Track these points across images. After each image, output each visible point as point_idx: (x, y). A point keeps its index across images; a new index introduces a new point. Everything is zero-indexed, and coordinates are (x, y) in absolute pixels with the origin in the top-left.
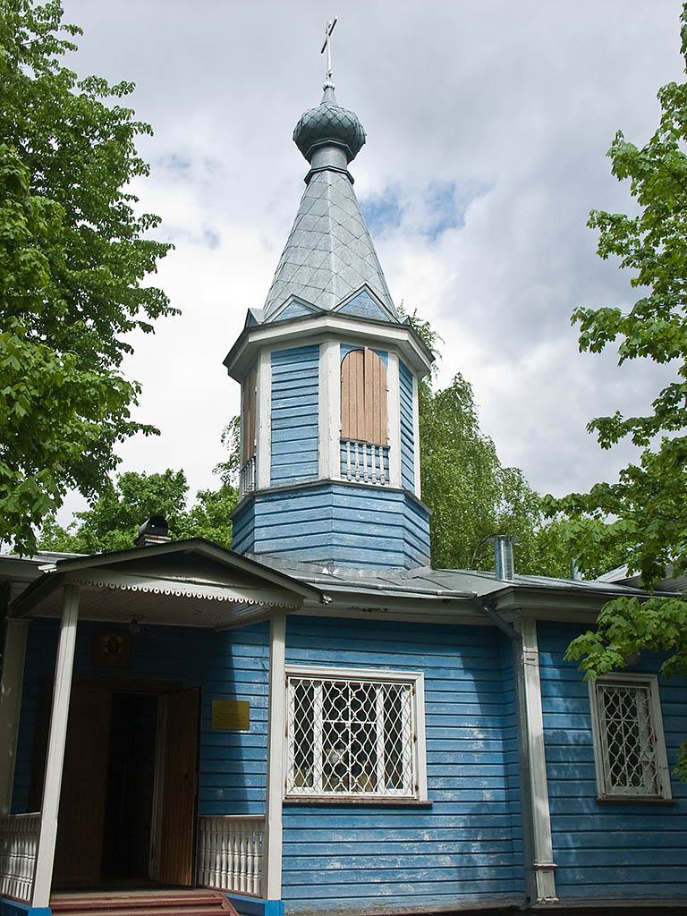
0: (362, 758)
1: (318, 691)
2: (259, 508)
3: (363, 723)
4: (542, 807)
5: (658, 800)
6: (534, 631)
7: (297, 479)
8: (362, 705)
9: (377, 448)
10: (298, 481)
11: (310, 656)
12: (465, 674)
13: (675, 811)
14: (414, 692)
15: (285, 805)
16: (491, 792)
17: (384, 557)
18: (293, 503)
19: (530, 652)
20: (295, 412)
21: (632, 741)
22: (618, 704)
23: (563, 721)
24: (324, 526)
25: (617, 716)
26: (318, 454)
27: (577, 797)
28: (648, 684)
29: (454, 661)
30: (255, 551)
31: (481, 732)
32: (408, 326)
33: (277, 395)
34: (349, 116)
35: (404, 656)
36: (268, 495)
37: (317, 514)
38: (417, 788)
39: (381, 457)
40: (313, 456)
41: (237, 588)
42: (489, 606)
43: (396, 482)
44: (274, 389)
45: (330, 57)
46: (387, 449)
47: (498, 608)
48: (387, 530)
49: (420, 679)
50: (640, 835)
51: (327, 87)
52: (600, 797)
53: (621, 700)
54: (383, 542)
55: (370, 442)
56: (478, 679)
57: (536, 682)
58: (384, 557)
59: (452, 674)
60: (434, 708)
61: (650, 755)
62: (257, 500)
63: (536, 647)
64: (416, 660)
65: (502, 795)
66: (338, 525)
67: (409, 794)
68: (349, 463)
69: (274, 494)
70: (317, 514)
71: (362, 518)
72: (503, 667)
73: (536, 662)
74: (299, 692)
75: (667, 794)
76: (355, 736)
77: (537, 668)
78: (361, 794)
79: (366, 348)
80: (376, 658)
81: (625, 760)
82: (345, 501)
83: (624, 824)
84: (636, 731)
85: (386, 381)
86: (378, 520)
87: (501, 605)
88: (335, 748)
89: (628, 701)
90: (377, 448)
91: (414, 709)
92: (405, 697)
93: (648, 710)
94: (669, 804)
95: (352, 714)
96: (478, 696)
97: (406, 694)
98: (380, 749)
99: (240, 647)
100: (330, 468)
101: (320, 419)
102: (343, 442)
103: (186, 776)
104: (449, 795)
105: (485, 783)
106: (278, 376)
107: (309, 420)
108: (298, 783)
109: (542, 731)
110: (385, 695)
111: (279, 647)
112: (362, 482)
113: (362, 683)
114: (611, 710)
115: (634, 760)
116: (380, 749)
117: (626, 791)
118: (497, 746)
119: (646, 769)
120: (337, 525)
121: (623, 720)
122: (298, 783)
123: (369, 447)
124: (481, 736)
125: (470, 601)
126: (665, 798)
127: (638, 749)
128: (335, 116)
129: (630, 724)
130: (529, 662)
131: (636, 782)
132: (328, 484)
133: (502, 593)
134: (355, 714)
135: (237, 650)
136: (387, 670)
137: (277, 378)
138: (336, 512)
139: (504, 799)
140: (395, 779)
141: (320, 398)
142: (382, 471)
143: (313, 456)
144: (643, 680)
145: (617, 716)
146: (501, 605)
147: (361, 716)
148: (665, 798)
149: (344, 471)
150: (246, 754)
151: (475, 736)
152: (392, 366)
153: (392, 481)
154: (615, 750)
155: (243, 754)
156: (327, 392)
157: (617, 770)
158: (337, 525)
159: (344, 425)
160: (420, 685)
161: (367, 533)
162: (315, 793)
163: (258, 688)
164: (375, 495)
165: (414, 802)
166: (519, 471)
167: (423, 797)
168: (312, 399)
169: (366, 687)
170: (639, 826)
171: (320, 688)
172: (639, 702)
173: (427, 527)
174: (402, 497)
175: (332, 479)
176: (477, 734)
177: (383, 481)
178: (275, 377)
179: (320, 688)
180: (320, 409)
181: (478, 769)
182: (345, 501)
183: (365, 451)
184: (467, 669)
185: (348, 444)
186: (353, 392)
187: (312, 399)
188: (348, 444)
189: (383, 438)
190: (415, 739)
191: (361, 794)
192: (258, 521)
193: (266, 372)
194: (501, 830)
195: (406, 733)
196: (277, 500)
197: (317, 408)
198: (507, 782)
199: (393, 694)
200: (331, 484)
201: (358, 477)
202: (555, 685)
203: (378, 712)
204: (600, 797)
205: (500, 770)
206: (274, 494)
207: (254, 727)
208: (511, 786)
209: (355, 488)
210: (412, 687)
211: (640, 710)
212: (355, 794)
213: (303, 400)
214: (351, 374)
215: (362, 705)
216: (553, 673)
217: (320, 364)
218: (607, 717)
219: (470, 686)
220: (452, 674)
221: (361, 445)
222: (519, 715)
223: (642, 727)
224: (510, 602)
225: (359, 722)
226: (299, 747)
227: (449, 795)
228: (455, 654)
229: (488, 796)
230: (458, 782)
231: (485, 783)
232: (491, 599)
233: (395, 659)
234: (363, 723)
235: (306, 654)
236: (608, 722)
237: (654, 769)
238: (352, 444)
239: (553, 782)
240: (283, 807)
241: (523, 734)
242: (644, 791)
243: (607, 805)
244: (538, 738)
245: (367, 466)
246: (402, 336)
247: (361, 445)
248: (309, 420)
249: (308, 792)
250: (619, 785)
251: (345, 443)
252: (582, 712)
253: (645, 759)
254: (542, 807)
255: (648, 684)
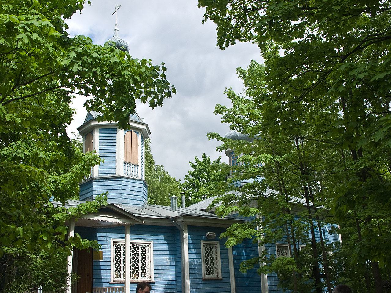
0: (135, 268)
1: (140, 248)
2: (94, 184)
3: (135, 257)
4: (188, 282)
5: (218, 279)
6: (187, 228)
7: (108, 174)
8: (135, 251)
9: (135, 165)
10: (109, 176)
11: (120, 236)
12: (165, 241)
13: (222, 282)
14: (150, 247)
15: (131, 283)
16: (171, 277)
17: (137, 202)
18: (107, 183)
19: (185, 235)
20: (108, 151)
21: (212, 261)
22: (210, 251)
23: (194, 256)
24: (118, 191)
25: (208, 254)
26: (116, 167)
27: (197, 279)
28: (216, 244)
29: (162, 237)
30: (93, 198)
31: (169, 259)
32: (143, 124)
33: (101, 144)
34: (125, 43)
35: (148, 236)
36: (98, 180)
37: (116, 187)
38: (151, 277)
39: (136, 168)
40: (114, 167)
41: (120, 219)
42: (174, 221)
43: (140, 178)
44: (100, 142)
45: (117, 18)
46: (138, 166)
47: (177, 221)
48: (138, 193)
49: (152, 242)
50: (213, 289)
51: (116, 30)
52: (203, 278)
53: (209, 249)
54: (136, 197)
55: (133, 163)
56: (169, 243)
57: (187, 244)
58: (137, 202)
59: (161, 242)
60: (156, 252)
61: (216, 265)
62: (94, 181)
63: (187, 233)
64: (151, 237)
65: (174, 279)
66: (123, 191)
67: (148, 279)
68: (126, 170)
69: (100, 179)
70: (116, 187)
71: (131, 189)
72: (175, 239)
73: (187, 238)
74: (117, 248)
75: (220, 277)
76: (133, 261)
77: (187, 240)
78: (134, 279)
79: (132, 131)
80: (140, 236)
81: (209, 268)
82: (125, 183)
83: (209, 286)
84: (213, 259)
85: (138, 142)
86: (135, 190)
87: (178, 221)
88: (135, 265)
89: (211, 250)
90: (135, 165)
91: (150, 253)
92: (147, 248)
93: (216, 252)
94: (221, 280)
95: (132, 254)
96: (168, 248)
97: (148, 248)
98: (140, 265)
99: (100, 233)
100: (120, 171)
101: (117, 155)
102: (125, 163)
103: (88, 275)
104: (160, 279)
105: (170, 275)
106: (102, 138)
107: (113, 154)
108: (117, 276)
109: (188, 259)
110: (141, 248)
111: (128, 236)
112: (130, 177)
113: (135, 245)
114: (207, 252)
115: (212, 267)
116: (140, 265)
117: (210, 276)
118: (173, 264)
119: (215, 269)
120: (123, 191)
121: (210, 255)
122: (117, 276)
123: (132, 165)
124: (169, 261)
125: (168, 219)
126: (220, 278)
127: (213, 264)
128: (121, 43)
129: (212, 256)
130: (185, 238)
131: (212, 274)
132: (120, 177)
133: (178, 217)
134: (133, 254)
135: (99, 234)
136: (142, 240)
137: (101, 138)
138: (123, 187)
139: (175, 280)
140: (145, 274)
141: (117, 147)
142: (136, 173)
143: (114, 167)
144: (215, 243)
145: (208, 254)
146: (178, 221)
147: (135, 255)
148: (220, 278)
149: (125, 173)
150: (102, 268)
151: (166, 260)
152: (140, 136)
153: (139, 177)
154: (207, 264)
155: (101, 268)
156: (120, 145)
157: (208, 270)
158: (123, 191)
159: (125, 157)
160: (152, 245)
161: (132, 194)
162: (121, 280)
163: (105, 246)
164: (135, 181)
165: (150, 282)
166: (162, 166)
167: (153, 280)
168: (114, 147)
169: (136, 246)
170: (212, 286)
171: (123, 246)
172: (214, 250)
173: (147, 191)
174: (142, 182)
175: (121, 176)
176: (168, 260)
177: (136, 176)
178: (100, 138)
179: (123, 246)
180: (117, 151)
181: (168, 271)
182: (125, 183)
183: (129, 166)
184: (165, 240)
185: (126, 164)
186: (128, 146)
187: (114, 147)
188: (126, 164)
189: (137, 162)
190: (150, 262)
191: (134, 279)
192: (94, 188)
193: (97, 136)
194: (174, 289)
195: (147, 261)
196: (101, 181)
197: (116, 151)
198: (176, 275)
199: (144, 248)
200: (121, 178)
201: (129, 175)
202: (192, 245)
203: (139, 254)
204: (203, 278)
205: (174, 271)
206: (100, 179)
207: (104, 259)
208: (177, 276)
209: (129, 179)
210: (149, 246)
211: (214, 252)
212: (133, 279)
213: (110, 147)
214: (127, 139)
215: (135, 251)
216: (191, 241)
217: (117, 135)
218: (205, 254)
219: (166, 245)
220: (161, 242)
221: (130, 164)
222: (182, 254)
223: (215, 257)
224: (182, 220)
225: (134, 257)
226: (117, 265)
227: (160, 279)
228: (162, 235)
229: (170, 279)
230: (162, 275)
231: (170, 275)
232: (175, 219)
233: (145, 237)
234: (135, 257)
235: (136, 236)
236: (206, 256)
237: (217, 270)
238: (128, 164)
239: (191, 274)
240: (130, 284)
241: (183, 260)
242: (214, 276)
243: (205, 281)
244: (187, 262)
245: (132, 172)
246: (144, 127)
247: (130, 164)
248: (113, 154)
249: (119, 279)
250: (208, 275)
251: (125, 163)
252: (199, 254)
253: (215, 267)
254: (188, 282)
255: (216, 244)
